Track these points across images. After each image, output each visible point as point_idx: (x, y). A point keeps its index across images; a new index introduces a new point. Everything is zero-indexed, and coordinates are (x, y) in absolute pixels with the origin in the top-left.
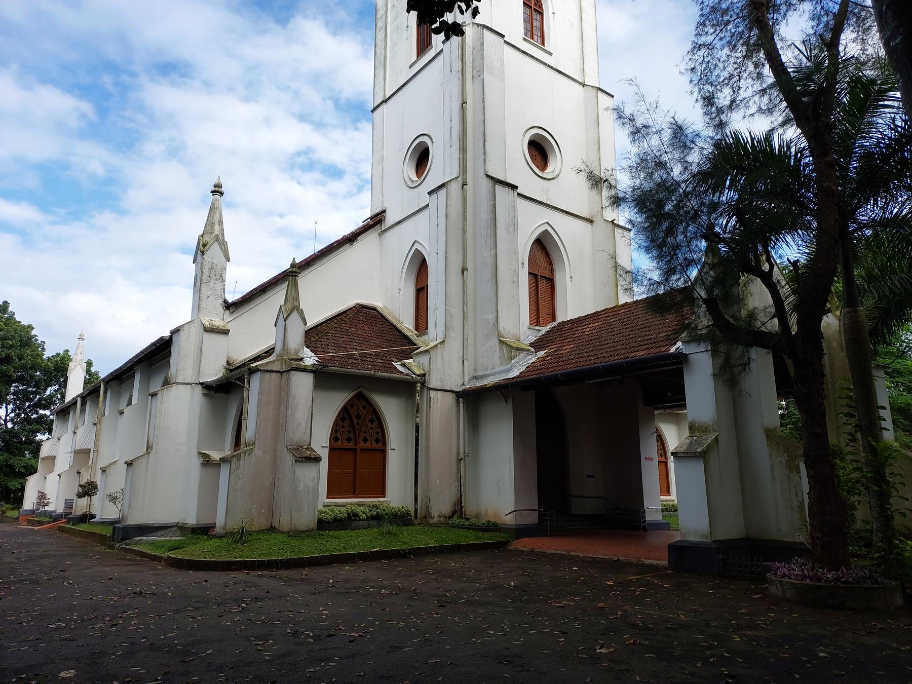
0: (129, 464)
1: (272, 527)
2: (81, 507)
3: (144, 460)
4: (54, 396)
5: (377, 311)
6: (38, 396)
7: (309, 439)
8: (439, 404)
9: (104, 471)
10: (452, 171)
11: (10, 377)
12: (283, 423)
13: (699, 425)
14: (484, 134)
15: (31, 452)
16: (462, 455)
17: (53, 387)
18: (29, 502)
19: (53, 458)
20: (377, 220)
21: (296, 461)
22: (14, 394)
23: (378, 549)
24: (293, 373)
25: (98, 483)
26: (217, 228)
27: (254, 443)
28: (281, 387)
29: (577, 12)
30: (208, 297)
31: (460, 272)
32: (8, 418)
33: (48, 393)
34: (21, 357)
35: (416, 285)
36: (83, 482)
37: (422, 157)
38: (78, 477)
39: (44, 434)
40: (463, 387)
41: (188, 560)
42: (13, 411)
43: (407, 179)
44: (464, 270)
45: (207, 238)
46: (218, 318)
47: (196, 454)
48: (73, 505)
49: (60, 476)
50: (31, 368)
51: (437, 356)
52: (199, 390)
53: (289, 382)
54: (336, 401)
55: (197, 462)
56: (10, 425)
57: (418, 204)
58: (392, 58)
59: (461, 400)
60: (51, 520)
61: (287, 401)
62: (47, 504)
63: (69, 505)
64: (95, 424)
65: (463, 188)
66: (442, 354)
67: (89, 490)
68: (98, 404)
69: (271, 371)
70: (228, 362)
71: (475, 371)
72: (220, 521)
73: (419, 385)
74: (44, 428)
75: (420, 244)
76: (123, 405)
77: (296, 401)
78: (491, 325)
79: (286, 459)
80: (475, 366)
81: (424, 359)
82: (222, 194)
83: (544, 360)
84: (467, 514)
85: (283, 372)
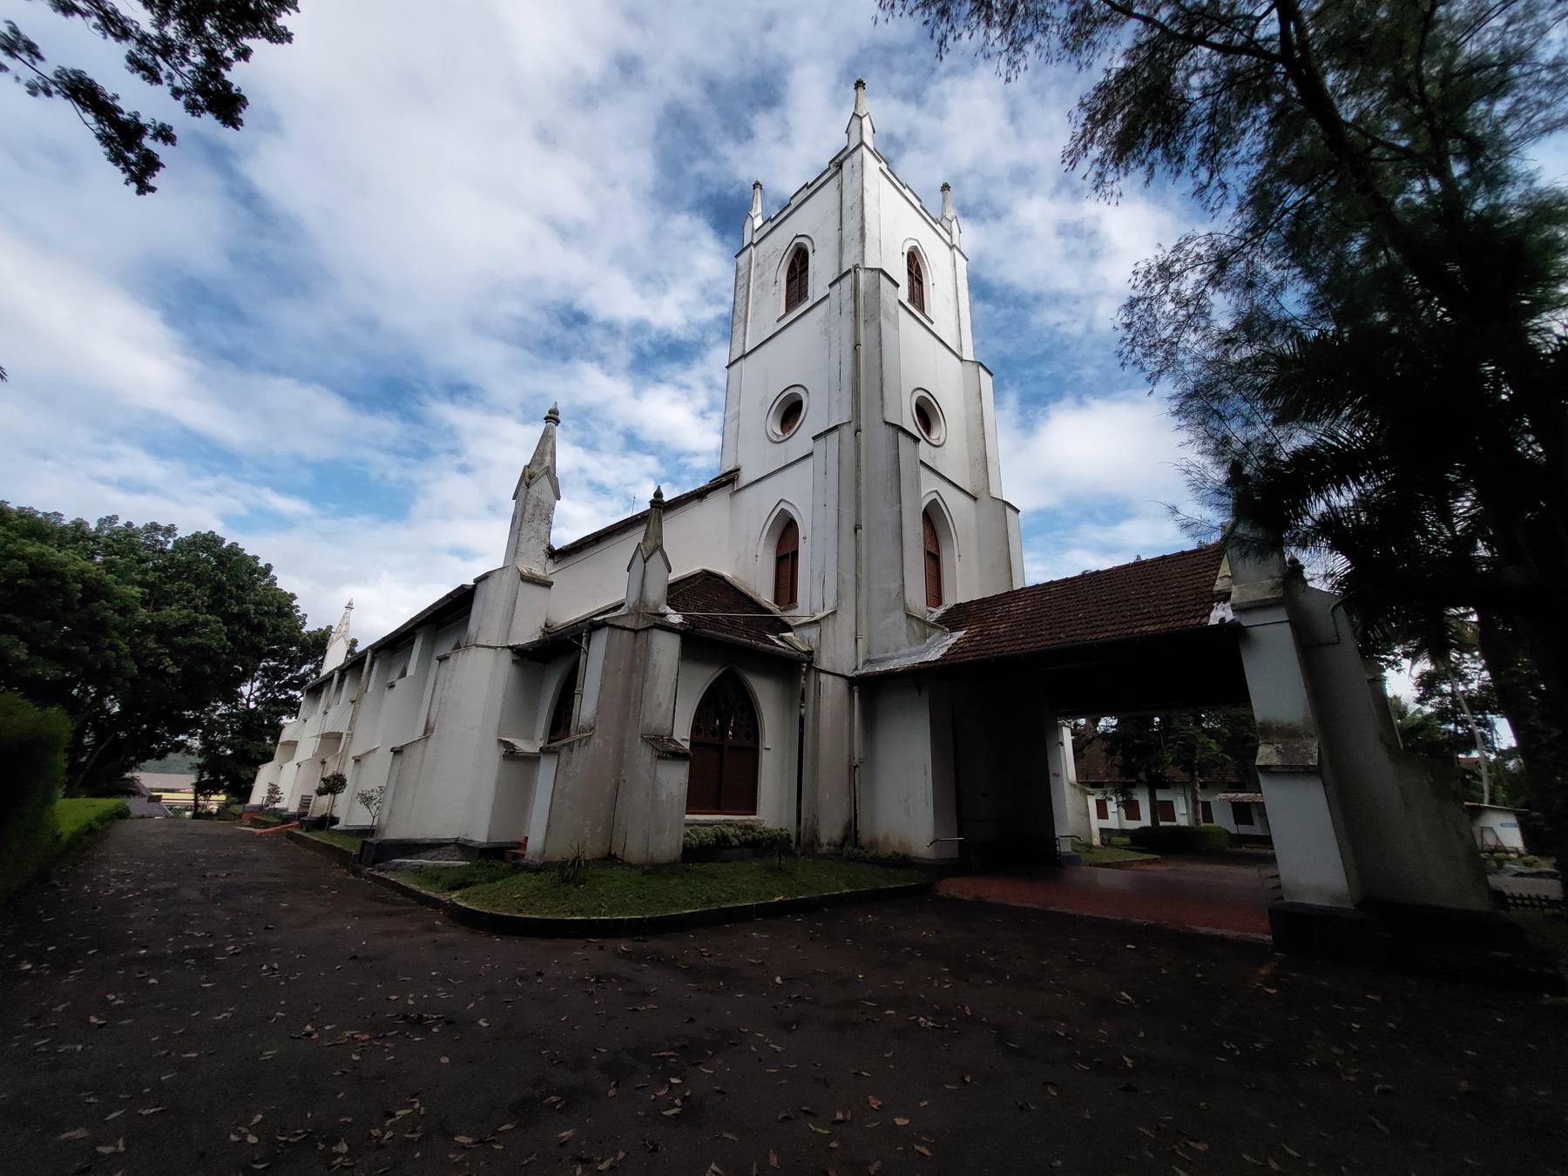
0: (397, 752)
1: (609, 854)
2: (321, 805)
3: (420, 746)
4: (308, 675)
5: (725, 581)
6: (290, 674)
7: (671, 727)
8: (830, 691)
9: (357, 760)
10: (843, 414)
11: (259, 649)
12: (636, 702)
13: (1277, 727)
14: (881, 379)
15: (272, 738)
16: (856, 761)
17: (309, 666)
18: (258, 796)
19: (295, 744)
20: (727, 481)
21: (659, 757)
22: (263, 670)
23: (781, 898)
24: (655, 631)
25: (348, 777)
26: (548, 458)
27: (593, 729)
28: (634, 651)
29: (952, 290)
30: (529, 540)
31: (853, 529)
32: (252, 697)
33: (302, 671)
34: (276, 629)
35: (779, 548)
36: (328, 774)
37: (790, 411)
38: (321, 769)
39: (291, 718)
40: (857, 672)
41: (491, 914)
42: (259, 689)
43: (770, 433)
44: (857, 528)
45: (534, 469)
46: (537, 566)
47: (495, 741)
48: (309, 804)
49: (299, 766)
50: (286, 641)
51: (828, 628)
52: (507, 656)
53: (648, 644)
54: (703, 678)
55: (495, 754)
56: (252, 705)
57: (786, 460)
58: (754, 314)
59: (855, 688)
60: (280, 821)
61: (645, 669)
62: (278, 801)
63: (305, 802)
64: (352, 702)
65: (856, 435)
66: (834, 628)
67: (333, 785)
68: (360, 679)
69: (624, 628)
70: (546, 625)
71: (869, 653)
72: (535, 841)
73: (805, 665)
74: (291, 710)
75: (788, 502)
76: (394, 676)
77: (657, 671)
78: (894, 596)
79: (640, 754)
80: (869, 647)
81: (812, 633)
82: (558, 422)
83: (972, 641)
84: (862, 841)
85: (639, 630)
